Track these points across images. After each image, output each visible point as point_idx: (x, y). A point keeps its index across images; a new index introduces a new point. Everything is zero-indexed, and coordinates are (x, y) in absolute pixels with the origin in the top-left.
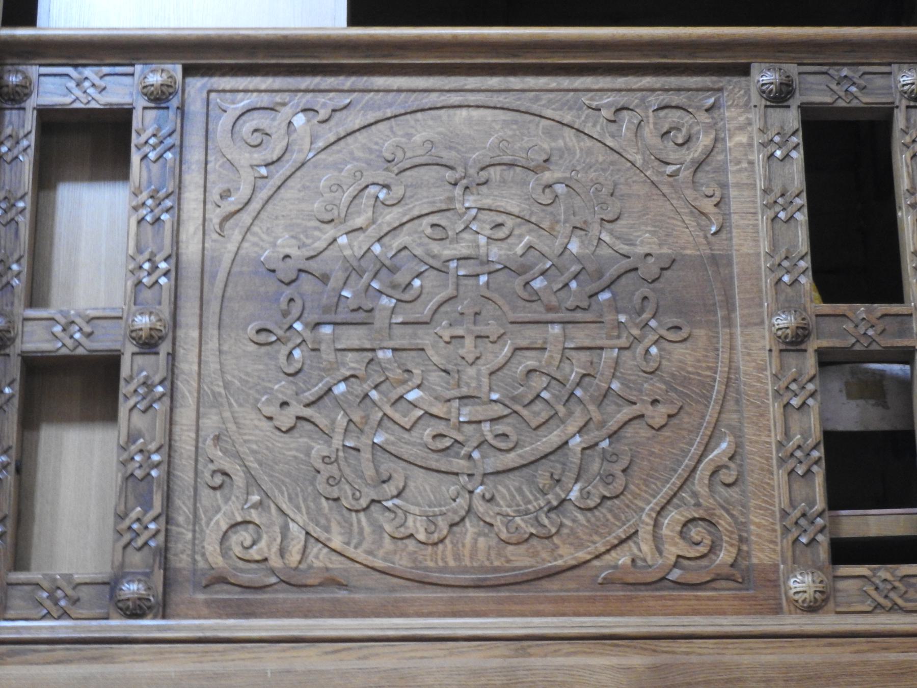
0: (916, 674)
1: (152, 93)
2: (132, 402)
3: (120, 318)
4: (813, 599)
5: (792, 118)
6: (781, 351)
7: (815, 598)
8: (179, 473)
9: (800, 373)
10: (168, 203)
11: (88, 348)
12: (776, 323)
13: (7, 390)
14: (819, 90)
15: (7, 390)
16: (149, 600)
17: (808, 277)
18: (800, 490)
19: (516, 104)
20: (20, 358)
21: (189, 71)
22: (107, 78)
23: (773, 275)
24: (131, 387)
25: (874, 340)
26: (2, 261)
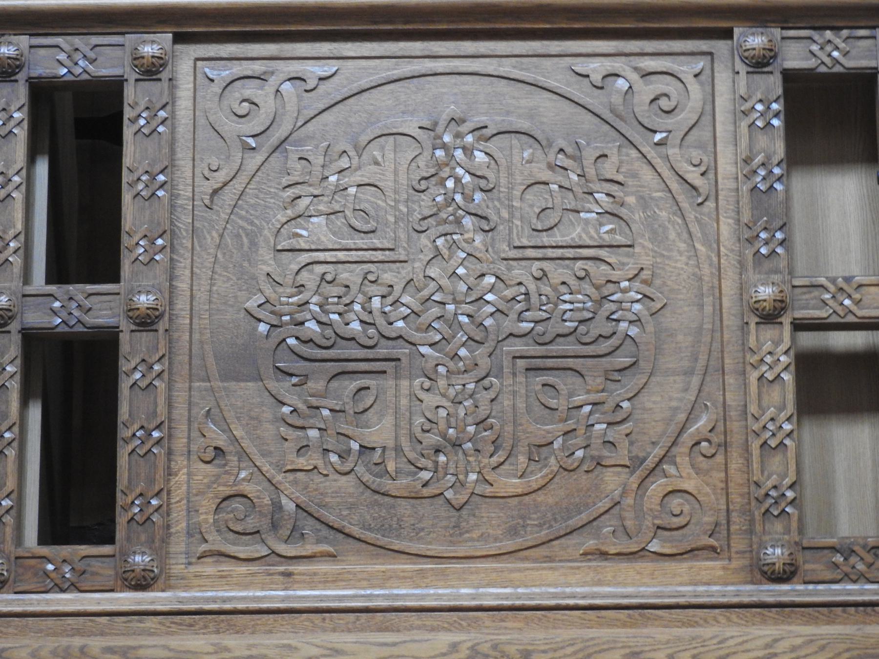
0: (878, 609)
1: (142, 65)
2: (130, 448)
3: (118, 294)
4: (772, 308)
5: (774, 84)
6: (748, 73)
7: (784, 570)
8: (176, 405)
9: (768, 157)
10: (162, 114)
11: (93, 74)
12: (754, 295)
13: (7, 435)
14: (799, 53)
15: (7, 435)
16: (153, 571)
17: (790, 373)
18: (762, 141)
19: (502, 71)
20: (20, 336)
21: (179, 38)
22: (92, 298)
23: (749, 182)
24: (129, 433)
25: (850, 311)
26: (2, 173)
